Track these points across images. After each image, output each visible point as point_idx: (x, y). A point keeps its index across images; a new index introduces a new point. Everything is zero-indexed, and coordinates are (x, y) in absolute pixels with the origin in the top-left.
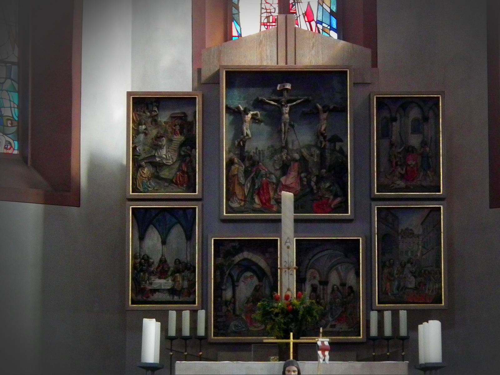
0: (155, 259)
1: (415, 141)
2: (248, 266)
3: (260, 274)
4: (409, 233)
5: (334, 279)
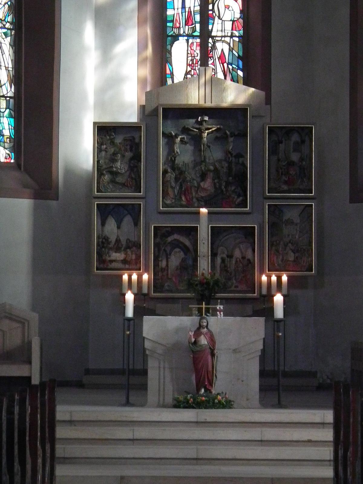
0: (113, 239)
1: (295, 157)
2: (177, 244)
3: (185, 249)
4: (290, 222)
5: (237, 254)
